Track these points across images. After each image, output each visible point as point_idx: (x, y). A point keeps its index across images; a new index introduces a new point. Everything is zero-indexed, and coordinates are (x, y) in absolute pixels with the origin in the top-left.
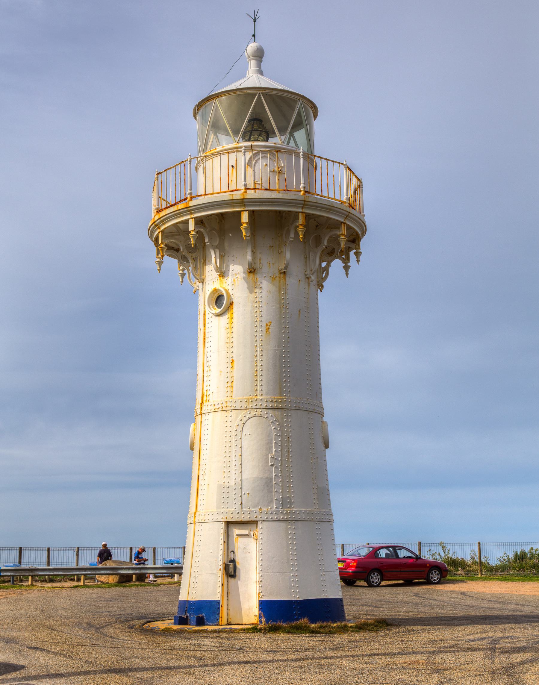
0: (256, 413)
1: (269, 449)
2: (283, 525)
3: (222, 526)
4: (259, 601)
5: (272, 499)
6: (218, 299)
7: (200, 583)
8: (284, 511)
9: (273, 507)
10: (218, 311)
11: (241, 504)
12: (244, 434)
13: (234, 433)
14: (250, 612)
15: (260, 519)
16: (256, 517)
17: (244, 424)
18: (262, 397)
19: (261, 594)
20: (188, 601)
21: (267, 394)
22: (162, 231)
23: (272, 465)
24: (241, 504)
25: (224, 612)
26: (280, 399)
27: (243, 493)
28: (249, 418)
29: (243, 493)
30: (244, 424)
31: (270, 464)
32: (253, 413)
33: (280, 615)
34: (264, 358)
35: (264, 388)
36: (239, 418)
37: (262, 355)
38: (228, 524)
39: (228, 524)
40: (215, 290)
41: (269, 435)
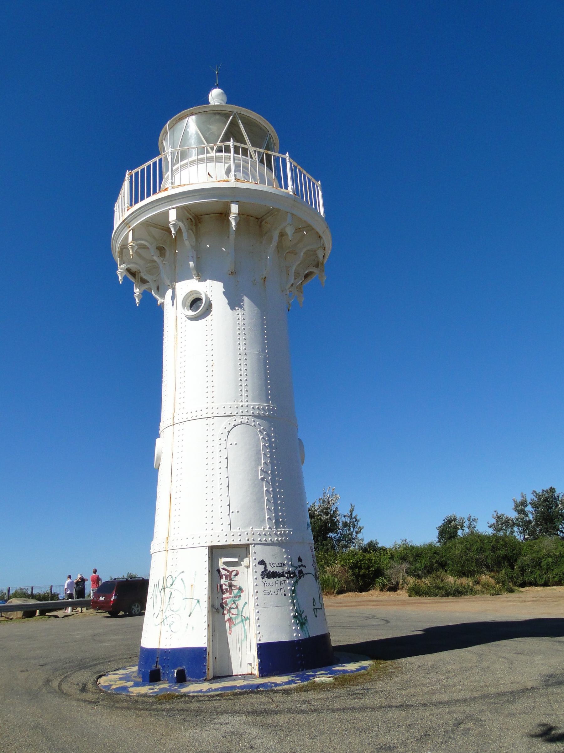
0: (242, 420)
1: (259, 460)
2: (277, 549)
3: (206, 551)
4: (258, 644)
5: (265, 517)
6: (195, 302)
7: (173, 621)
8: (278, 531)
9: (266, 526)
10: (191, 313)
11: (230, 524)
12: (229, 443)
13: (217, 443)
14: (245, 660)
15: (253, 542)
16: (248, 540)
17: (229, 432)
18: (248, 403)
19: (260, 635)
20: (159, 649)
21: (253, 400)
22: (133, 230)
23: (262, 479)
24: (230, 524)
25: (209, 662)
26: (267, 406)
27: (231, 511)
28: (235, 426)
29: (231, 511)
30: (229, 432)
31: (260, 477)
32: (239, 421)
33: (273, 657)
34: (248, 362)
35: (249, 393)
36: (223, 426)
37: (246, 359)
38: (212, 549)
39: (212, 549)
40: (192, 292)
41: (258, 445)
